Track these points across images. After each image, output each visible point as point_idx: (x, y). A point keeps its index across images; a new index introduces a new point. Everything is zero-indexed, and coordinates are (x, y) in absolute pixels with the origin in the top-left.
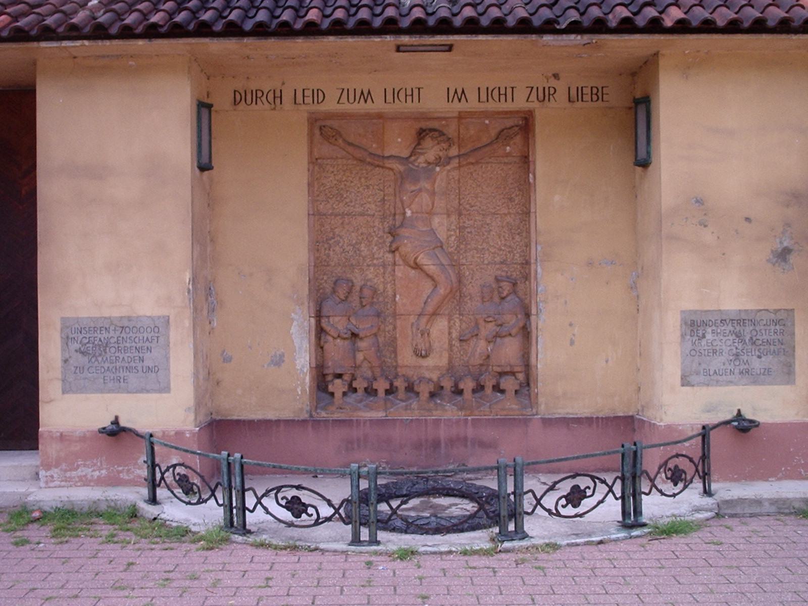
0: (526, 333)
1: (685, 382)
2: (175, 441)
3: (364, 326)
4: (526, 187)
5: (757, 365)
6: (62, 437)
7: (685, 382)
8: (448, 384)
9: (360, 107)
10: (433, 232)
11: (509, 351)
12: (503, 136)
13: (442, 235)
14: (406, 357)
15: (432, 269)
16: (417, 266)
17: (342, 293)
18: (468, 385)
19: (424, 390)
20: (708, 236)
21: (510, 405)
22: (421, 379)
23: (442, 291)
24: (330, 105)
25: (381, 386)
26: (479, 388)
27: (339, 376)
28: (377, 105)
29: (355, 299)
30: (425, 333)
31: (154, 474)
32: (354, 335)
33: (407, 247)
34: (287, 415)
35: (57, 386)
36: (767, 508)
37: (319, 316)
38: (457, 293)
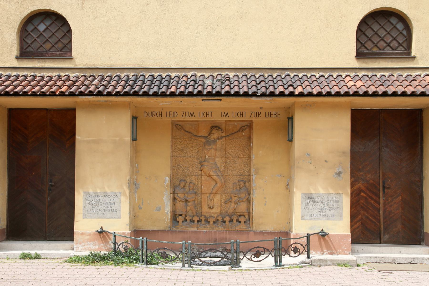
0: (249, 201)
1: (303, 218)
2: (123, 236)
3: (190, 197)
4: (250, 149)
5: (329, 213)
6: (82, 234)
7: (303, 218)
8: (220, 219)
9: (190, 119)
10: (215, 163)
11: (242, 208)
12: (242, 129)
13: (219, 165)
14: (205, 209)
15: (215, 177)
16: (210, 176)
17: (182, 185)
18: (227, 219)
19: (211, 221)
20: (312, 167)
21: (243, 226)
22: (210, 216)
23: (218, 185)
24: (179, 118)
25: (196, 219)
26: (231, 221)
27: (181, 215)
28: (196, 118)
29: (187, 188)
30: (212, 200)
31: (115, 247)
32: (187, 201)
33: (206, 169)
34: (162, 228)
35: (81, 216)
36: (329, 263)
37: (174, 193)
38: (224, 186)
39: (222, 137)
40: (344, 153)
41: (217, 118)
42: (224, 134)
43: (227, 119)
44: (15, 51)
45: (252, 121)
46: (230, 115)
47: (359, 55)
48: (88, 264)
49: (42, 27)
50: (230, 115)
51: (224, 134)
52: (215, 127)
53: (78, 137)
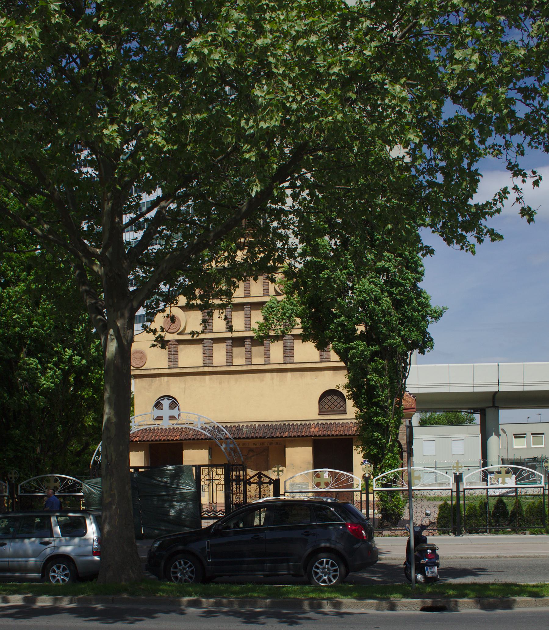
20: (294, 470)
39: (254, 455)
40: (309, 463)
47: (321, 413)
52: (251, 450)
53: (184, 459)
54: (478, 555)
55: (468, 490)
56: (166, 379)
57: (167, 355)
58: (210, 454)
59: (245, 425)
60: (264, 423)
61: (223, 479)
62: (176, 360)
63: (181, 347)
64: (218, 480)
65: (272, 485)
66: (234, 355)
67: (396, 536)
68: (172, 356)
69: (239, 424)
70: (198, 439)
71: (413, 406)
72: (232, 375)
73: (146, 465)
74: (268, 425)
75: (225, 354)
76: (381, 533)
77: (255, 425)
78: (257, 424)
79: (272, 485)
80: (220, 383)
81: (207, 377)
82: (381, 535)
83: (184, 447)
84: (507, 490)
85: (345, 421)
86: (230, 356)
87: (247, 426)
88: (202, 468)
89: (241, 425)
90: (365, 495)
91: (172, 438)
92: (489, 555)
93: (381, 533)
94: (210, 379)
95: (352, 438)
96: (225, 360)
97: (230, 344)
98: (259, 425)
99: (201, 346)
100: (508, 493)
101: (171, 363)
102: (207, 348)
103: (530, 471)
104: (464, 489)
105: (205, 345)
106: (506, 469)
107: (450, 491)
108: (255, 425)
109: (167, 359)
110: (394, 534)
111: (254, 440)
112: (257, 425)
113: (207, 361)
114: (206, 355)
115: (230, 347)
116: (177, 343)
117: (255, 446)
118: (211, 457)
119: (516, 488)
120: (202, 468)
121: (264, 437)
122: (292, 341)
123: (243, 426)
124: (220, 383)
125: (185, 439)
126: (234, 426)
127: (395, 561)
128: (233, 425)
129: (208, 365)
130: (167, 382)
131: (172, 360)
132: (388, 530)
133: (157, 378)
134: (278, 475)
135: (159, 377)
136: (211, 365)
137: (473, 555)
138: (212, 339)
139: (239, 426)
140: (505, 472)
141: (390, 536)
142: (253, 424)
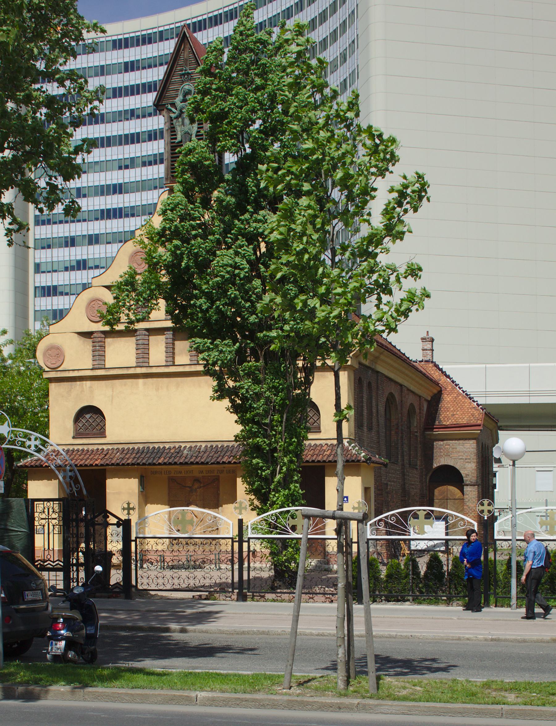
24: (172, 475)
28: (183, 475)
39: (201, 487)
41: (196, 474)
42: (202, 485)
43: (202, 475)
44: (72, 434)
45: (219, 476)
46: (204, 472)
48: (186, 682)
49: (88, 416)
50: (204, 472)
51: (202, 485)
52: (197, 480)
54: (314, 632)
55: (253, 540)
56: (88, 383)
57: (91, 352)
58: (142, 484)
59: (188, 446)
60: (212, 443)
61: (36, 519)
62: (103, 358)
63: (108, 340)
64: (42, 519)
65: (121, 527)
66: (176, 351)
67: (282, 601)
68: (97, 353)
69: (181, 444)
70: (123, 465)
71: (479, 422)
72: (172, 379)
73: (62, 496)
74: (217, 446)
75: (165, 349)
76: (263, 597)
77: (201, 446)
78: (204, 445)
79: (121, 527)
80: (157, 390)
81: (141, 381)
82: (263, 599)
83: (108, 474)
84: (436, 542)
85: (318, 442)
86: (171, 353)
87: (191, 447)
88: (36, 503)
89: (183, 445)
90: (356, 544)
91: (91, 463)
92: (328, 632)
93: (263, 597)
94: (145, 384)
95: (105, 469)
96: (164, 358)
97: (171, 336)
98: (206, 446)
99: (134, 339)
100: (435, 546)
101: (95, 363)
102: (140, 342)
103: (458, 517)
104: (249, 538)
105: (138, 338)
106: (426, 512)
107: (231, 540)
108: (201, 446)
109: (91, 357)
110: (279, 598)
111: (201, 466)
112: (203, 446)
113: (141, 360)
114: (139, 352)
115: (170, 341)
116: (103, 336)
117: (201, 475)
118: (143, 488)
119: (447, 541)
120: (36, 503)
121: (207, 463)
122: (146, 337)
123: (185, 447)
124: (157, 390)
125: (107, 465)
126: (174, 447)
127: (243, 636)
128: (172, 445)
129: (141, 364)
130: (91, 387)
131: (97, 358)
132: (273, 593)
133: (78, 383)
134: (129, 514)
135: (80, 381)
136: (147, 365)
137: (308, 631)
138: (147, 330)
139: (180, 447)
140: (240, 518)
141: (274, 600)
142: (199, 444)
